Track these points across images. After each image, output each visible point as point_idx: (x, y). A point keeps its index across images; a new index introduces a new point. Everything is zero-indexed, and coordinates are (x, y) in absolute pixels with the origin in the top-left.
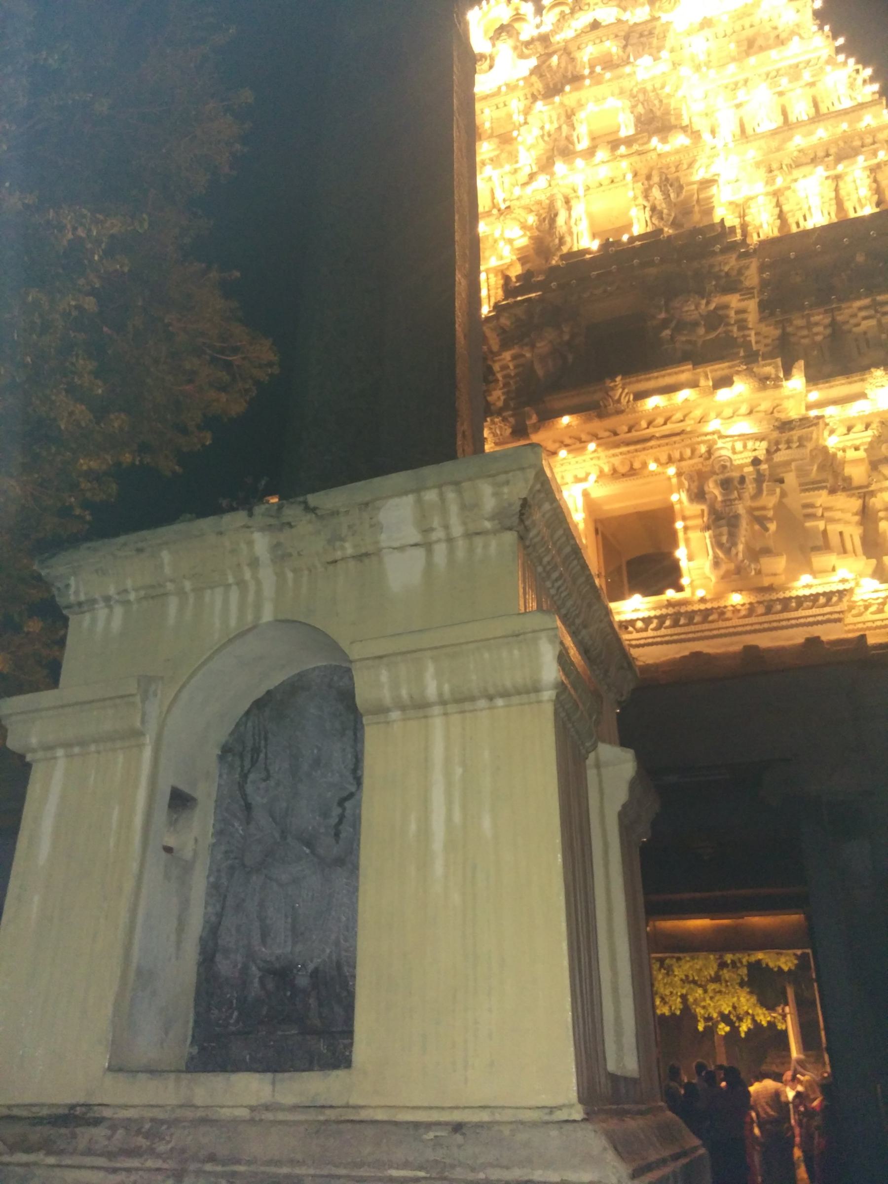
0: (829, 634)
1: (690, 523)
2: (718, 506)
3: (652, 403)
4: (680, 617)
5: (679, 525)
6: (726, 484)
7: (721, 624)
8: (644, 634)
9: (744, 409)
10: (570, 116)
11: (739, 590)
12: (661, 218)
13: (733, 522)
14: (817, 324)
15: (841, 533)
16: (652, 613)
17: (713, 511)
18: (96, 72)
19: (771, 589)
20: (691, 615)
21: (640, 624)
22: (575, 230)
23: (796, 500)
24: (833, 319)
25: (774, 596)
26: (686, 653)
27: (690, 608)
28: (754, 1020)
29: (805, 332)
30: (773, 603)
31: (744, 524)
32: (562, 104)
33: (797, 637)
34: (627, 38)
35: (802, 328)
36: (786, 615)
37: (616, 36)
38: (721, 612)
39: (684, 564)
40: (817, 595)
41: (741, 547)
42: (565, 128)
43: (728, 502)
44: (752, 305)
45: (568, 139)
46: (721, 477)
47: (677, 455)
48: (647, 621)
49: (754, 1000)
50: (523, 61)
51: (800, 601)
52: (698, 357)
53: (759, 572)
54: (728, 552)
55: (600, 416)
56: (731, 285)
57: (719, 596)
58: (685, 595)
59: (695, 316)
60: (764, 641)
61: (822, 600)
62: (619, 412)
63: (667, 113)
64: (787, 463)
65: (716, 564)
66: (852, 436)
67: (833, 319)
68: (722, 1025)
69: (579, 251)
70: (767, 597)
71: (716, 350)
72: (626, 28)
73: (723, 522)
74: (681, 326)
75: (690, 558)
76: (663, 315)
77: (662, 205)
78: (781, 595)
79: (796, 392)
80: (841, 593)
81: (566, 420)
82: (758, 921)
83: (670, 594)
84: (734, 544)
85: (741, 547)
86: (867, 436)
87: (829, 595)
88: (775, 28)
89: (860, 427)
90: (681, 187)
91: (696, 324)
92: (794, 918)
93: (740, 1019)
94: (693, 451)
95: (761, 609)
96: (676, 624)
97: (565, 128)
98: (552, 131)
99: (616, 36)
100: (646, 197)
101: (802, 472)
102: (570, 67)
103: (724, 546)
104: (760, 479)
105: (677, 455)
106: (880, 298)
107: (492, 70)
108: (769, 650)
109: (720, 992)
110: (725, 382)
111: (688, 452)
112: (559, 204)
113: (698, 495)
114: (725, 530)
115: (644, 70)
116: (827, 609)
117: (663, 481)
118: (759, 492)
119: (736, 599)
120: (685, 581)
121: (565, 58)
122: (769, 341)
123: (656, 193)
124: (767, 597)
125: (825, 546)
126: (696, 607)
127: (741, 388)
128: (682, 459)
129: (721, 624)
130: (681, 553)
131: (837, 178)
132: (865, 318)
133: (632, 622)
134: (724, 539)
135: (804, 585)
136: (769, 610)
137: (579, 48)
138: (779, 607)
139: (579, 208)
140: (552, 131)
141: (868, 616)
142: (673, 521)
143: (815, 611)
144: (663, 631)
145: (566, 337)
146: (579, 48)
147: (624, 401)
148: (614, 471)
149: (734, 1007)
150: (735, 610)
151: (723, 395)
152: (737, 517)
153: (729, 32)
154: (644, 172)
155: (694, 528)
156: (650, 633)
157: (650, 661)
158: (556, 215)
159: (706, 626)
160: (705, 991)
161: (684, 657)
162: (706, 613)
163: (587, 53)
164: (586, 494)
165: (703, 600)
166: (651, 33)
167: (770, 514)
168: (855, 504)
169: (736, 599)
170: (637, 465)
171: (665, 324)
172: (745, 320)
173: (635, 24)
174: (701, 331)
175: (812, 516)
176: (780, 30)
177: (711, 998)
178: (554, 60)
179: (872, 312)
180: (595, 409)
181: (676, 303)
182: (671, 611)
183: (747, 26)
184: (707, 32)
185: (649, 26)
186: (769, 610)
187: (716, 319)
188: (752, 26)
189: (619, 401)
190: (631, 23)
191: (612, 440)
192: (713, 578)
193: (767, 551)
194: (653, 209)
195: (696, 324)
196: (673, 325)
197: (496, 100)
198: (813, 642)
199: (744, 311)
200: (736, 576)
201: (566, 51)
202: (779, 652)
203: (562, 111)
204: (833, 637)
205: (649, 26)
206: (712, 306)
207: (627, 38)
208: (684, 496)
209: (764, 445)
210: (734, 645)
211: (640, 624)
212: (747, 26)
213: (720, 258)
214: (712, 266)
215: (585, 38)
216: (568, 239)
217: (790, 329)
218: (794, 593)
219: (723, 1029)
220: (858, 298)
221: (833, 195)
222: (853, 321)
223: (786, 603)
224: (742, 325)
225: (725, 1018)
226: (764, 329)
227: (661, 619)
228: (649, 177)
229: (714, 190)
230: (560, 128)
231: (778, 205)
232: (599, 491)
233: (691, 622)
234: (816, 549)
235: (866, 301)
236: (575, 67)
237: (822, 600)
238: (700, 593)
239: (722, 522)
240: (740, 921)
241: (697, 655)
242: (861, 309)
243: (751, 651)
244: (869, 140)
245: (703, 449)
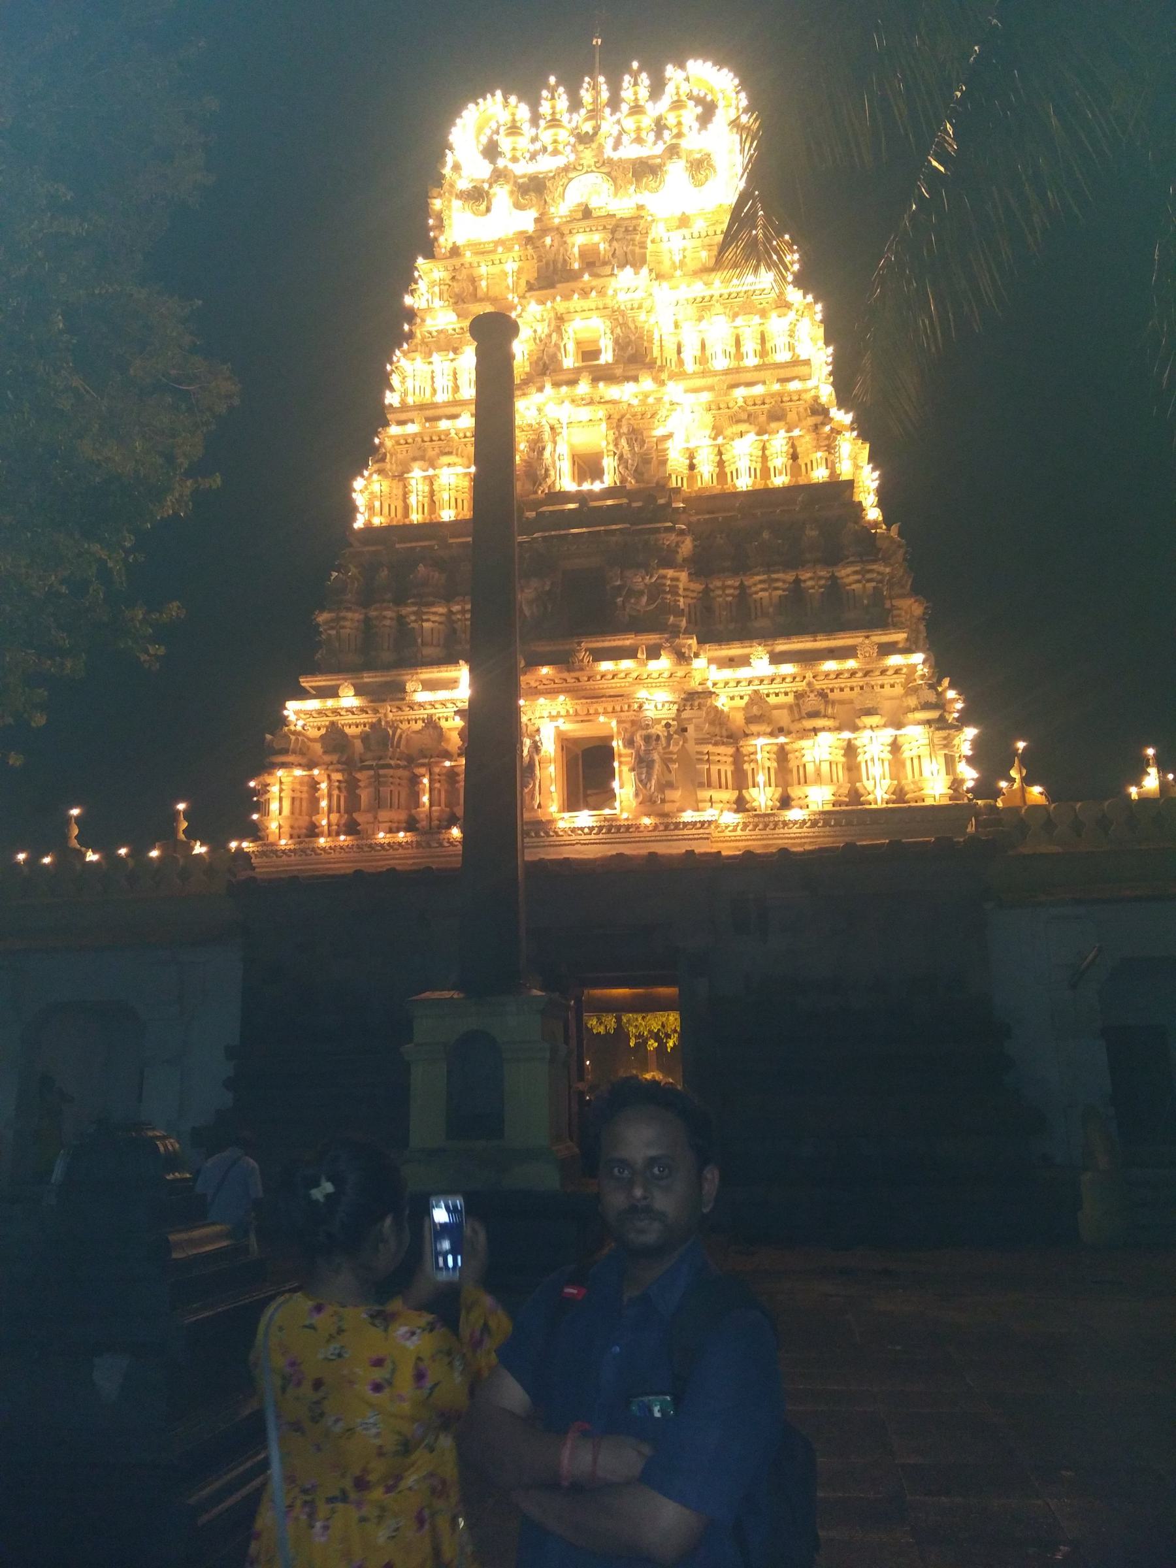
0: (701, 848)
2: (642, 753)
4: (611, 827)
6: (647, 739)
7: (637, 834)
8: (589, 837)
10: (560, 319)
11: (648, 815)
12: (627, 468)
13: (650, 765)
15: (719, 771)
17: (638, 755)
21: (586, 830)
23: (692, 747)
24: (742, 583)
30: (668, 825)
31: (657, 767)
34: (613, 232)
35: (718, 588)
36: (677, 832)
37: (605, 228)
39: (617, 791)
41: (653, 782)
42: (554, 336)
43: (648, 752)
45: (557, 346)
47: (618, 708)
48: (591, 829)
50: (518, 211)
51: (685, 824)
53: (663, 801)
54: (645, 785)
56: (668, 561)
57: (637, 818)
59: (641, 587)
60: (661, 849)
61: (699, 825)
62: (582, 669)
64: (690, 719)
65: (637, 795)
66: (739, 688)
68: (651, 1042)
70: (666, 820)
72: (614, 222)
74: (632, 593)
75: (621, 787)
76: (618, 583)
77: (627, 455)
78: (674, 820)
79: (704, 669)
80: (710, 822)
81: (545, 670)
83: (607, 811)
84: (649, 780)
85: (653, 782)
87: (703, 823)
91: (641, 593)
93: (668, 1036)
95: (662, 828)
96: (609, 832)
97: (554, 336)
98: (543, 336)
99: (605, 228)
101: (698, 728)
104: (669, 737)
105: (618, 708)
106: (774, 576)
108: (663, 856)
111: (626, 707)
112: (547, 435)
113: (629, 743)
114: (644, 770)
115: (625, 285)
116: (701, 831)
119: (646, 821)
120: (617, 804)
121: (557, 237)
123: (623, 442)
124: (666, 820)
126: (622, 823)
127: (664, 664)
129: (637, 834)
130: (616, 784)
132: (763, 590)
136: (666, 828)
138: (672, 827)
139: (563, 448)
140: (543, 336)
141: (727, 833)
143: (694, 831)
144: (601, 836)
145: (547, 588)
147: (586, 661)
148: (576, 714)
149: (663, 1026)
150: (646, 826)
151: (654, 666)
152: (653, 761)
153: (703, 234)
156: (593, 836)
157: (591, 856)
158: (544, 449)
159: (627, 835)
162: (628, 827)
164: (557, 727)
165: (627, 819)
169: (646, 821)
171: (620, 588)
172: (677, 587)
173: (622, 219)
180: (564, 661)
182: (606, 824)
186: (666, 828)
187: (656, 591)
190: (618, 217)
191: (575, 692)
193: (670, 785)
194: (621, 458)
195: (641, 593)
197: (491, 257)
198: (690, 853)
199: (677, 579)
200: (648, 803)
201: (559, 232)
202: (670, 858)
203: (552, 315)
204: (702, 850)
205: (634, 222)
209: (676, 707)
211: (586, 830)
213: (663, 535)
217: (711, 586)
218: (682, 820)
219: (653, 1044)
221: (760, 453)
224: (674, 591)
225: (656, 1037)
226: (693, 586)
227: (600, 828)
229: (669, 444)
230: (549, 336)
231: (720, 453)
232: (568, 727)
233: (618, 831)
234: (701, 785)
235: (765, 577)
237: (699, 825)
239: (643, 764)
241: (620, 855)
242: (761, 582)
243: (653, 855)
244: (795, 398)
245: (636, 706)
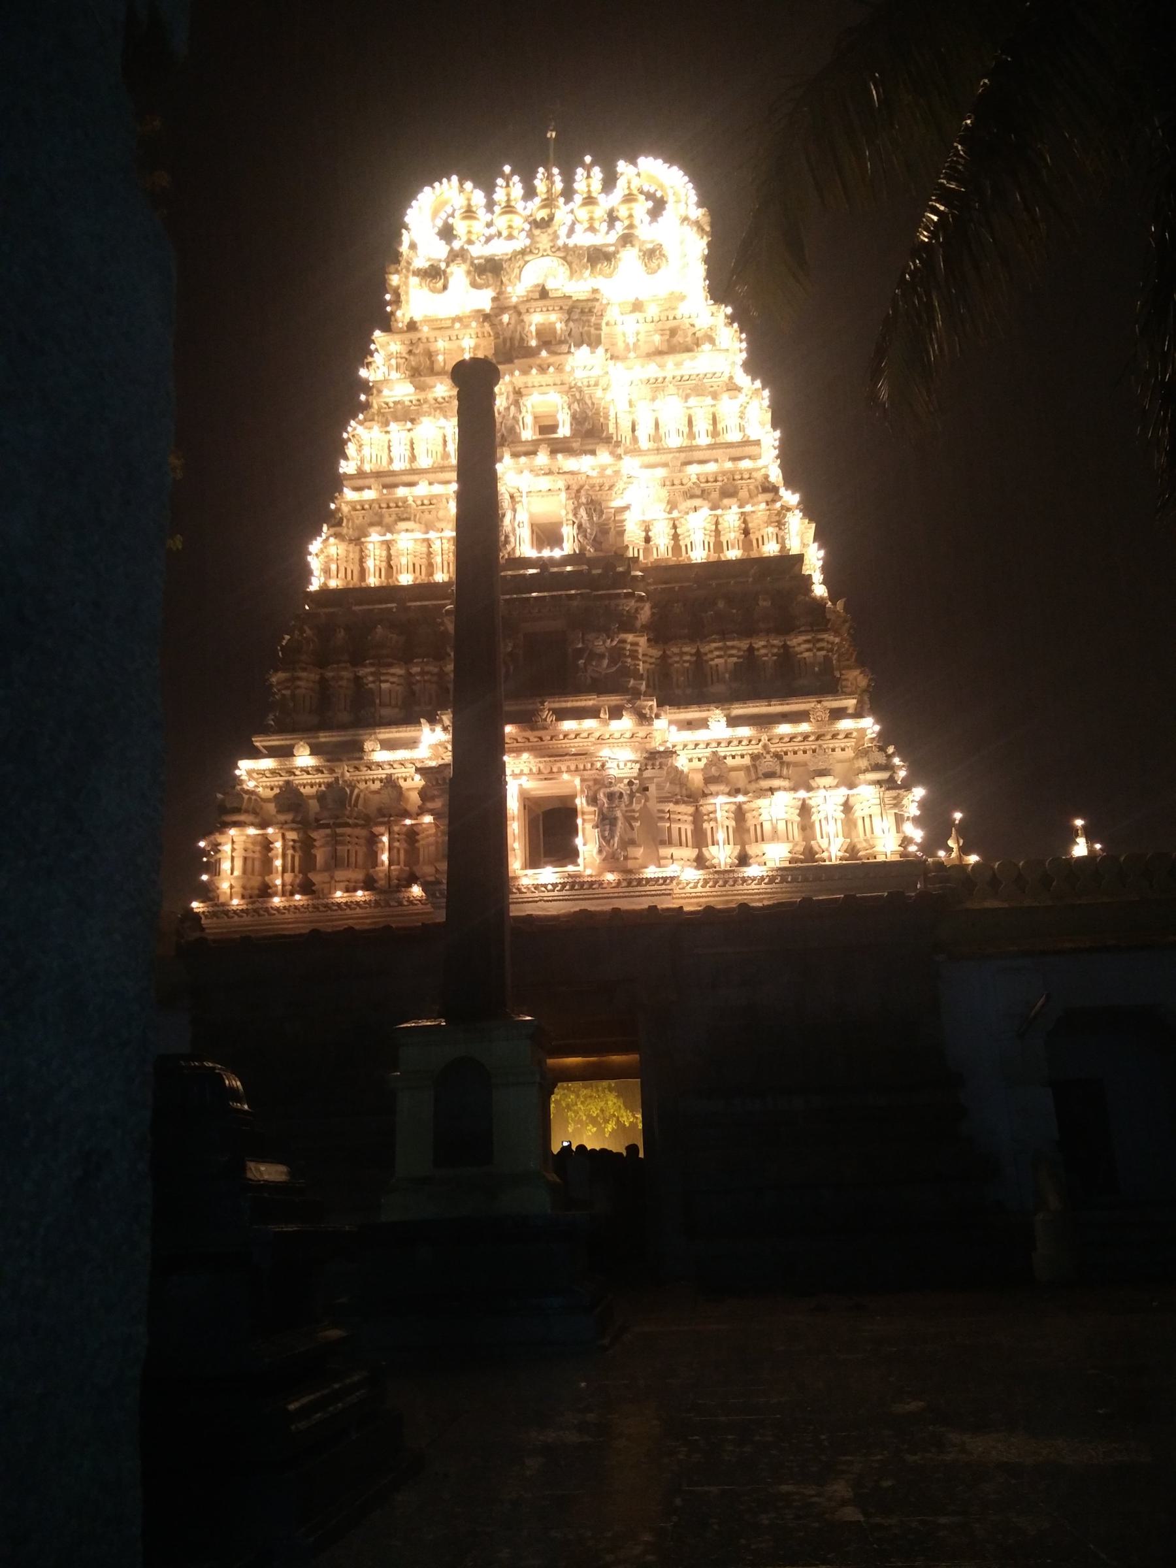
1: (586, 817)
2: (605, 810)
3: (568, 725)
4: (575, 884)
5: (579, 821)
6: (610, 796)
9: (628, 735)
11: (612, 871)
13: (613, 822)
14: (686, 653)
16: (558, 881)
17: (601, 813)
18: (416, 891)
19: (630, 872)
20: (582, 884)
21: (550, 887)
22: (518, 531)
23: (654, 806)
24: (698, 650)
25: (633, 877)
26: (577, 909)
27: (581, 880)
28: (618, 1122)
29: (677, 659)
30: (631, 880)
31: (620, 824)
32: (511, 382)
33: (643, 904)
36: (639, 888)
37: (561, 308)
38: (601, 884)
39: (581, 848)
40: (658, 878)
41: (616, 839)
43: (611, 809)
44: (643, 641)
46: (608, 790)
48: (555, 885)
49: (620, 1103)
51: (648, 881)
52: (599, 687)
53: (626, 858)
54: (608, 842)
55: (533, 729)
56: (627, 624)
57: (600, 874)
58: (580, 868)
59: (602, 650)
60: (625, 905)
61: (661, 881)
62: (545, 728)
63: (597, 413)
64: (651, 779)
65: (600, 851)
66: (697, 750)
67: (698, 650)
69: (520, 558)
71: (616, 687)
72: (570, 303)
73: (607, 822)
75: (585, 844)
77: (586, 524)
78: (637, 876)
80: (672, 878)
82: (616, 1058)
83: (570, 868)
84: (612, 837)
85: (616, 839)
86: (701, 765)
87: (665, 879)
88: (693, 325)
89: (702, 746)
90: (602, 512)
91: (602, 656)
92: (633, 1058)
93: (607, 1121)
94: (592, 765)
95: (624, 884)
96: (572, 889)
97: (512, 408)
100: (575, 515)
101: (659, 787)
102: (519, 328)
103: (606, 839)
104: (632, 795)
107: (446, 292)
108: (627, 912)
109: (591, 1097)
110: (616, 713)
111: (589, 766)
113: (593, 800)
115: (582, 362)
116: (664, 887)
117: (570, 782)
118: (631, 802)
121: (514, 317)
122: (653, 660)
123: (582, 512)
124: (629, 877)
125: (669, 843)
127: (626, 724)
128: (585, 769)
130: (579, 841)
131: (717, 517)
132: (719, 657)
133: (545, 886)
134: (607, 834)
135: (651, 872)
136: (629, 884)
137: (528, 311)
142: (576, 816)
144: (564, 893)
146: (528, 311)
147: (549, 720)
148: (540, 772)
149: (602, 1111)
150: (609, 883)
152: (616, 819)
153: (656, 319)
154: (575, 487)
155: (590, 821)
156: (556, 893)
160: (578, 1096)
161: (575, 912)
162: (592, 884)
163: (536, 319)
165: (591, 876)
166: (590, 311)
167: (637, 815)
168: (690, 809)
169: (610, 877)
170: (555, 770)
172: (637, 651)
174: (606, 662)
175: (662, 819)
176: (697, 328)
177: (582, 1103)
178: (505, 318)
179: (722, 653)
181: (590, 636)
182: (570, 880)
183: (671, 318)
184: (637, 315)
185: (590, 304)
186: (629, 884)
187: (617, 654)
188: (675, 318)
189: (545, 720)
190: (574, 299)
191: (539, 751)
192: (598, 859)
193: (632, 843)
194: (580, 526)
195: (602, 656)
196: (586, 655)
197: (449, 332)
199: (636, 644)
200: (612, 860)
203: (511, 389)
204: (665, 906)
205: (590, 304)
206: (615, 643)
207: (570, 312)
208: (584, 800)
209: (638, 766)
210: (606, 906)
211: (550, 887)
212: (671, 318)
213: (624, 601)
214: (618, 605)
215: (534, 304)
216: (512, 539)
217: (668, 652)
220: (714, 641)
222: (710, 656)
223: (640, 882)
227: (564, 885)
228: (578, 491)
234: (663, 843)
236: (524, 328)
237: (661, 881)
238: (588, 872)
239: (606, 821)
240: (604, 1059)
242: (717, 649)
245: (599, 765)
